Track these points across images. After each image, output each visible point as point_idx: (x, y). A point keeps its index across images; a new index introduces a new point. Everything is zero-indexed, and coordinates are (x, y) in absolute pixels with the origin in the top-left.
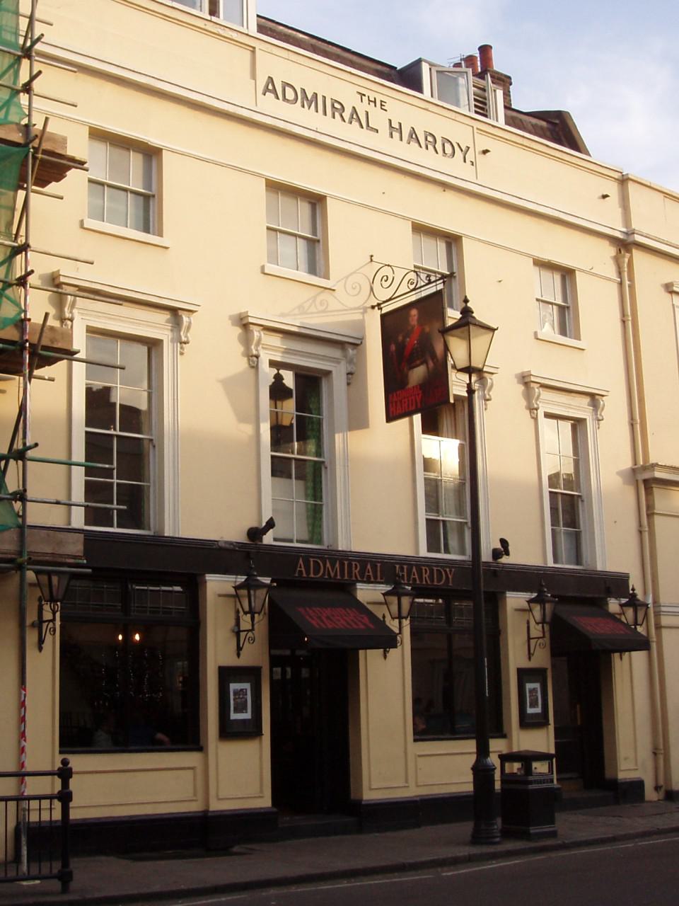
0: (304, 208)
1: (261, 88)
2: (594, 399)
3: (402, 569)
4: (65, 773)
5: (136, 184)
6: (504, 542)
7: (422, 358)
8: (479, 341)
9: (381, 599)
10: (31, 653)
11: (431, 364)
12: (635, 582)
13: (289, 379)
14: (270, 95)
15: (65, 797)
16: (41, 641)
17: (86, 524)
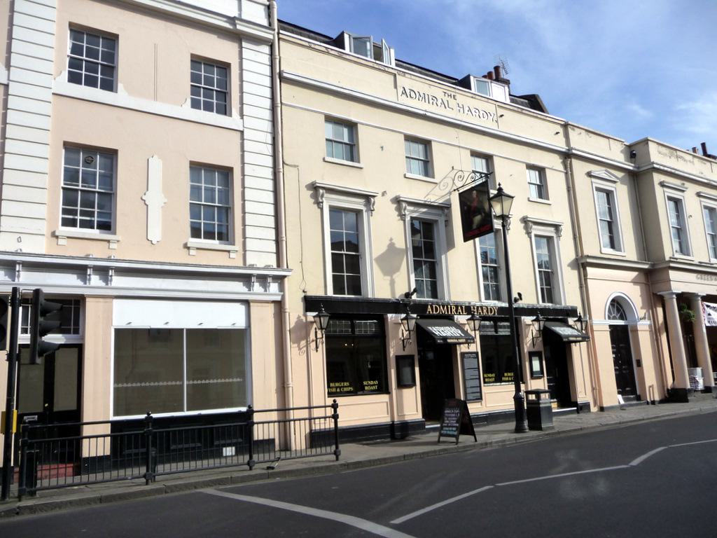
0: (421, 147)
1: (400, 93)
2: (557, 227)
3: (474, 308)
4: (335, 406)
5: (346, 140)
6: (520, 295)
7: (479, 210)
8: (506, 203)
9: (531, 323)
10: (313, 353)
11: (483, 214)
12: (580, 311)
13: (417, 225)
14: (404, 96)
15: (335, 417)
16: (317, 347)
17: (334, 293)
